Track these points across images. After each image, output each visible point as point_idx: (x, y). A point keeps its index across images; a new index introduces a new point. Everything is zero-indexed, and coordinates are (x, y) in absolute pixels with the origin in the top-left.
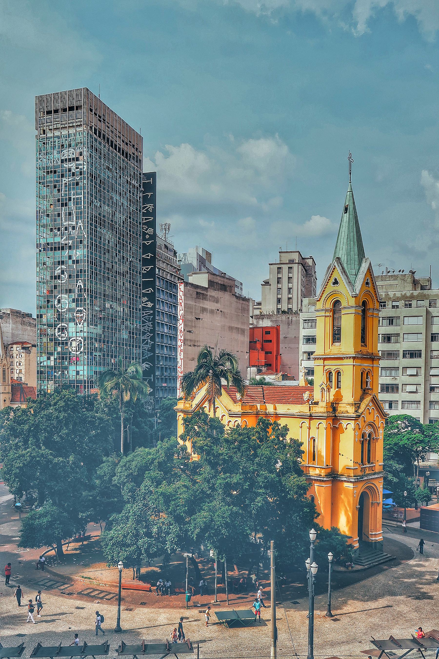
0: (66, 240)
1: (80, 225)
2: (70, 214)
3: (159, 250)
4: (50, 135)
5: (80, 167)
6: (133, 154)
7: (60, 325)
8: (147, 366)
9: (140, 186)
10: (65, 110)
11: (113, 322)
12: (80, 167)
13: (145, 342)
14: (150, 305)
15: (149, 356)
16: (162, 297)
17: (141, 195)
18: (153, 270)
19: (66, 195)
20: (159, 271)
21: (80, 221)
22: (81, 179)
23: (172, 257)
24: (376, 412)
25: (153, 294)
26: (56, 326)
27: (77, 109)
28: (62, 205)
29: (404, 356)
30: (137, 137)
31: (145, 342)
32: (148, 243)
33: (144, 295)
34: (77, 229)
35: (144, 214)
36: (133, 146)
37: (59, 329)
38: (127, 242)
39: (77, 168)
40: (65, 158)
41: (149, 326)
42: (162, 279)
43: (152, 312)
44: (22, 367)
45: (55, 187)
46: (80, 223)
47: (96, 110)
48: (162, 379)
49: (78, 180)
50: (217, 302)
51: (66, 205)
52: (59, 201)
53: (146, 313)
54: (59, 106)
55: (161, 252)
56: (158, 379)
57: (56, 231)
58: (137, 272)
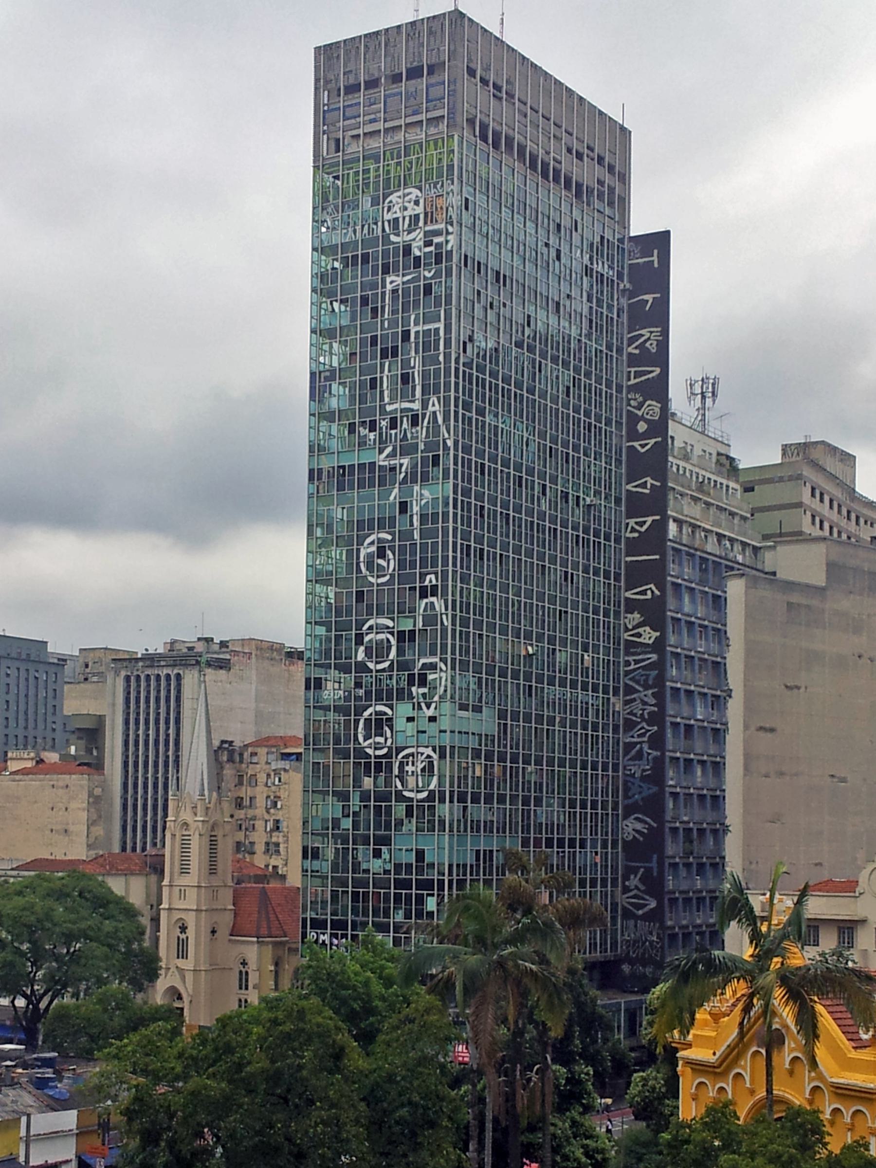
0: (392, 455)
1: (434, 409)
2: (406, 379)
3: (682, 464)
4: (354, 148)
5: (437, 240)
6: (601, 183)
7: (370, 710)
8: (639, 826)
9: (620, 276)
10: (396, 78)
11: (530, 695)
12: (437, 240)
13: (633, 752)
14: (649, 636)
15: (644, 794)
16: (687, 608)
17: (624, 302)
18: (660, 527)
19: (394, 323)
21: (434, 399)
22: (438, 274)
23: (725, 482)
25: (659, 603)
26: (359, 712)
27: (431, 72)
28: (384, 356)
30: (612, 131)
31: (633, 752)
32: (643, 446)
33: (631, 606)
34: (425, 424)
35: (633, 360)
36: (601, 160)
37: (368, 721)
38: (576, 448)
39: (428, 244)
40: (395, 216)
41: (645, 703)
42: (688, 554)
43: (654, 657)
44: (280, 813)
45: (365, 301)
46: (435, 406)
47: (487, 69)
48: (688, 866)
49: (431, 278)
50: (857, 629)
51: (395, 354)
52: (374, 339)
53: (637, 662)
54: (382, 66)
55: (689, 467)
56: (675, 866)
57: (364, 431)
58: (607, 538)
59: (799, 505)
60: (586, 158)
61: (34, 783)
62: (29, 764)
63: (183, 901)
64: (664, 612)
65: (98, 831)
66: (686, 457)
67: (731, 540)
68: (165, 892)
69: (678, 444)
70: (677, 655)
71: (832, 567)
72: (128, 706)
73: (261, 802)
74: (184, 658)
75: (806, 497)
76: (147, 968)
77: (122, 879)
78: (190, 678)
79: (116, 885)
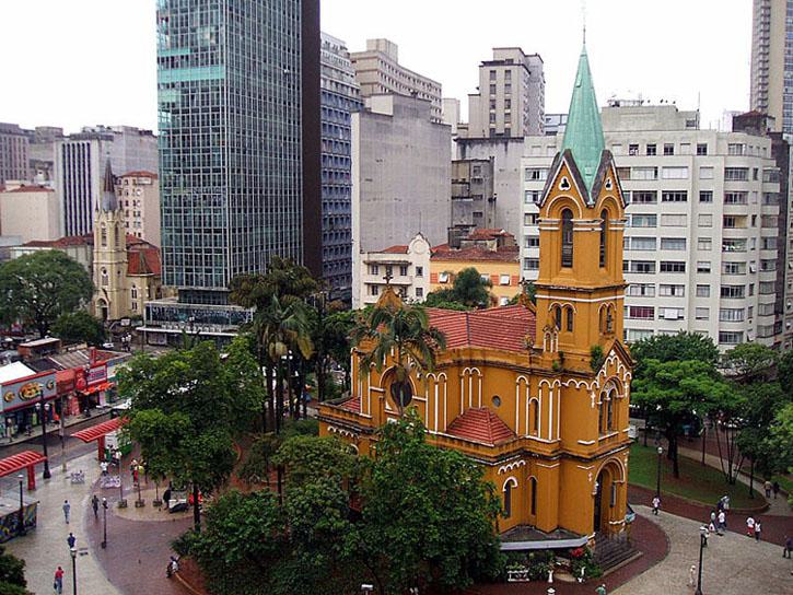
24: (619, 362)
63: (104, 259)
64: (319, 121)
66: (328, 48)
68: (95, 254)
69: (323, 42)
70: (324, 109)
71: (396, 107)
74: (90, 134)
76: (89, 290)
78: (94, 145)
79: (71, 253)
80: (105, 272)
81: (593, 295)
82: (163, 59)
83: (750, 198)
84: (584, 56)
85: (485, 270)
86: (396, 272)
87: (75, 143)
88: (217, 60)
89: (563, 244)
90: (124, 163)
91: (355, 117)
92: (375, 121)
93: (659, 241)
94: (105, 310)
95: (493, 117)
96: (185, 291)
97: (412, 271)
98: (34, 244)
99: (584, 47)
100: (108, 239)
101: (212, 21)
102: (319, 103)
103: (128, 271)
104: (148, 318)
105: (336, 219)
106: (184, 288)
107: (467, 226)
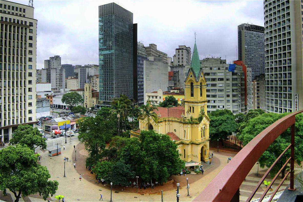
20: (140, 54)
24: (206, 120)
29: (218, 80)
59: (151, 51)
60: (128, 15)
61: (71, 80)
62: (70, 78)
65: (78, 85)
66: (139, 46)
67: (144, 55)
68: (85, 93)
69: (138, 45)
70: (138, 60)
71: (155, 59)
72: (80, 77)
73: (95, 81)
75: (152, 50)
77: (80, 92)
78: (87, 69)
80: (87, 97)
81: (199, 104)
82: (100, 49)
83: (238, 80)
84: (195, 45)
85: (176, 97)
86: (151, 97)
87: (83, 68)
88: (112, 49)
89: (191, 91)
90: (94, 73)
91: (145, 61)
92: (149, 62)
93: (217, 90)
94: (86, 106)
95: (179, 62)
96: (104, 102)
97: (158, 97)
98: (71, 90)
99: (195, 43)
100: (87, 89)
101: (111, 40)
102: (137, 58)
103: (92, 97)
104: (96, 108)
105: (141, 85)
106: (104, 101)
107: (172, 87)
